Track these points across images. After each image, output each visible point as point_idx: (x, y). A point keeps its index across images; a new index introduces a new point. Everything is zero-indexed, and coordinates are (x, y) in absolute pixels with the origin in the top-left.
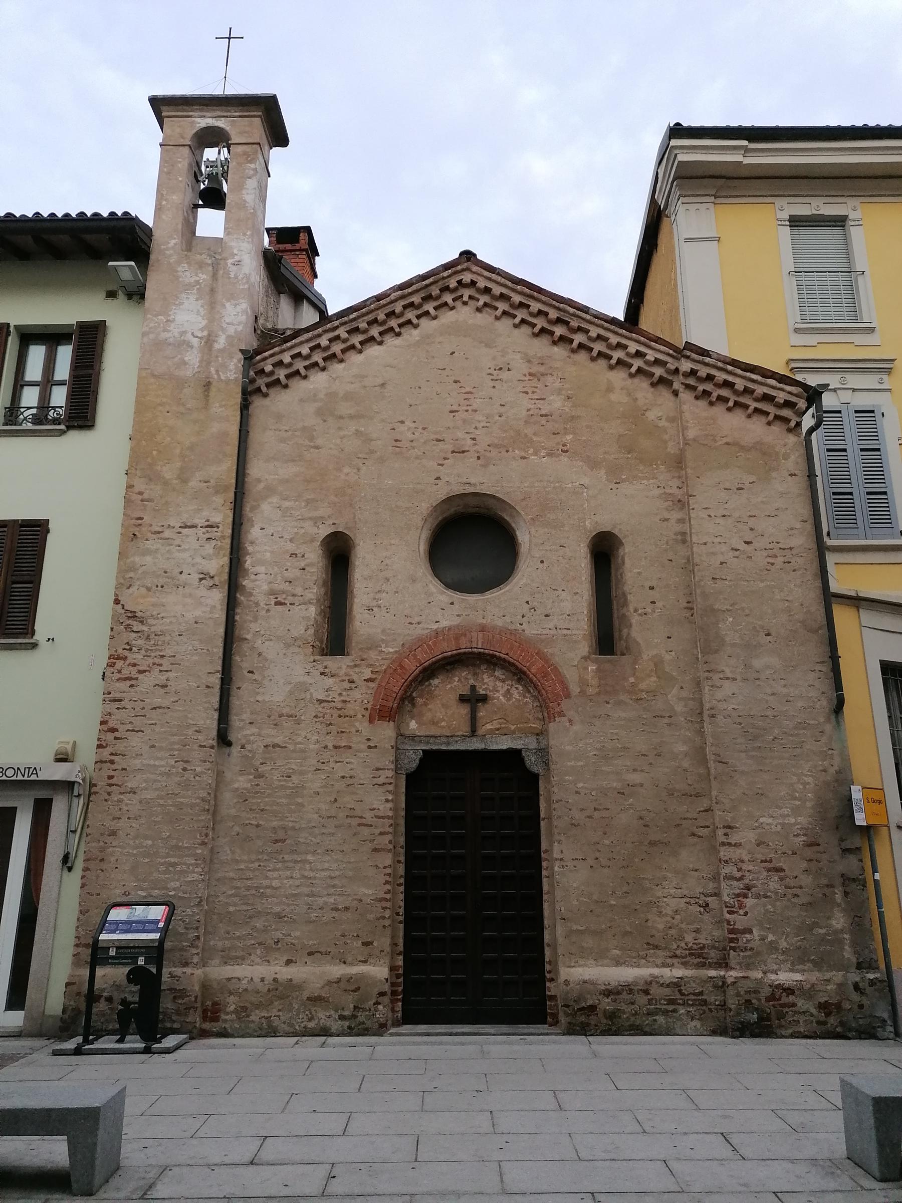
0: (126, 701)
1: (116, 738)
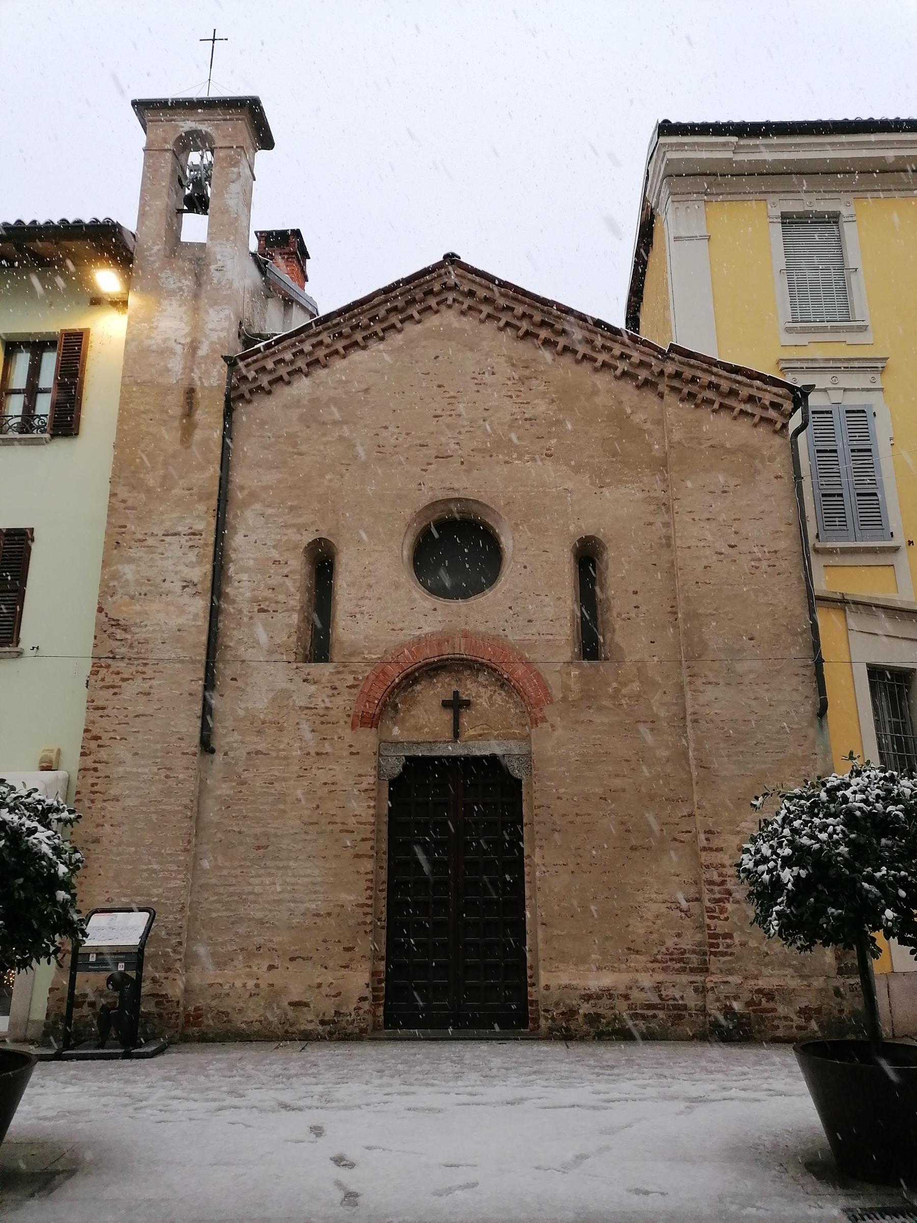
1: (99, 746)
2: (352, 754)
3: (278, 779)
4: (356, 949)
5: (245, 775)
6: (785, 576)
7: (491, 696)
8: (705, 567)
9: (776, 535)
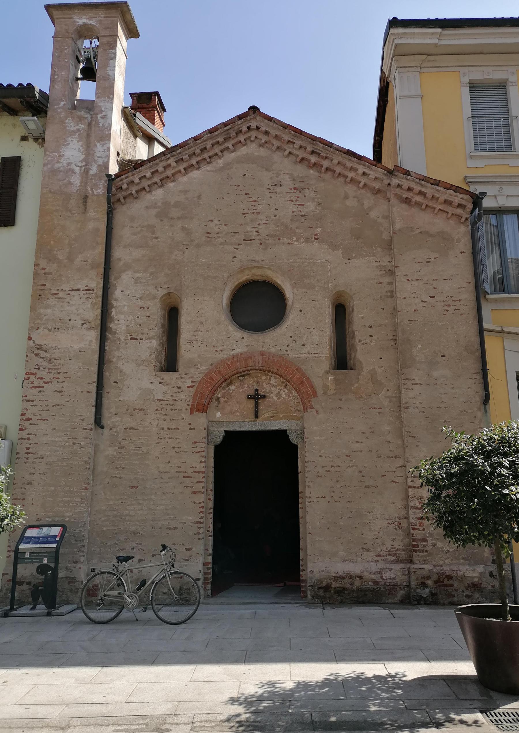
1: (31, 424)
2: (190, 429)
4: (194, 549)
5: (123, 443)
7: (279, 392)
8: (415, 311)
9: (460, 290)
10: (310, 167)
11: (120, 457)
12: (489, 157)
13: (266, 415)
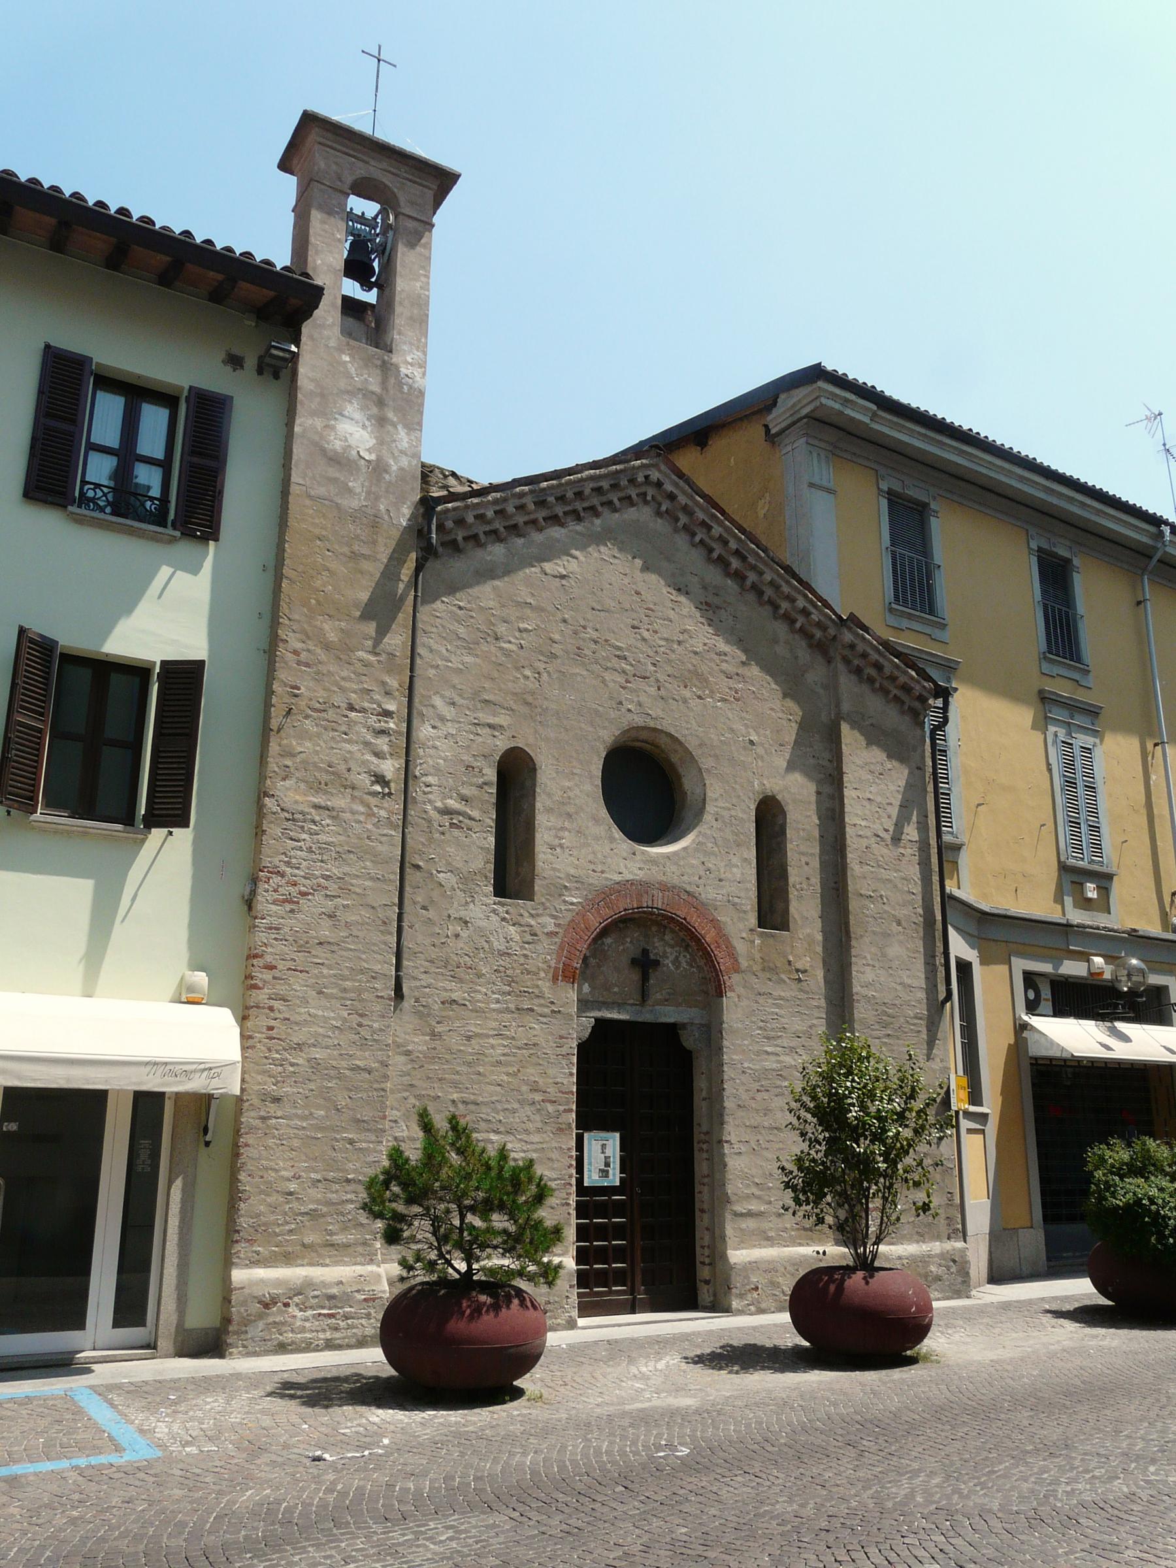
0: (287, 929)
1: (274, 978)
2: (553, 1012)
3: (477, 1035)
5: (439, 1029)
6: (565, 722)
7: (677, 957)
10: (728, 574)
11: (434, 1058)
12: (910, 617)
13: (658, 996)
